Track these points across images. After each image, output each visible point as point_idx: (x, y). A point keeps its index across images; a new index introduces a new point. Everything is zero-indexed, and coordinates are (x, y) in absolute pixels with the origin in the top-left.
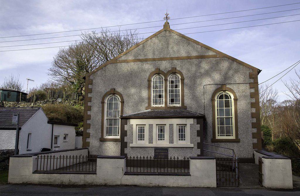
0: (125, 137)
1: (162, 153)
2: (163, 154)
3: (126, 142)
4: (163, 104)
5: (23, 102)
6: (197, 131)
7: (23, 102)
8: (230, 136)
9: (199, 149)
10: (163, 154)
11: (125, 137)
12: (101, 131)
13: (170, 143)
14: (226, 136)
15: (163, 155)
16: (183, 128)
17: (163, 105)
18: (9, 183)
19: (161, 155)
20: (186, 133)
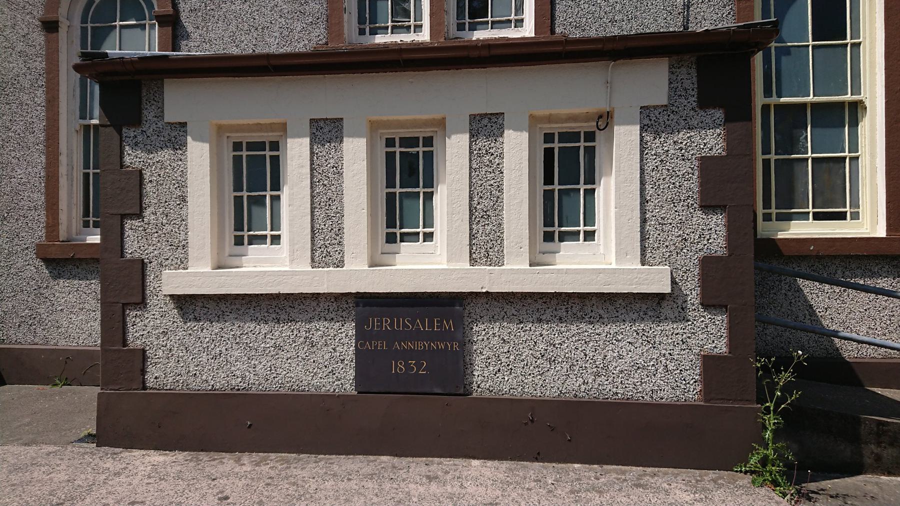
0: (128, 223)
1: (417, 336)
2: (420, 345)
3: (133, 261)
4: (418, 28)
5: (428, 130)
6: (703, 160)
7: (428, 130)
8: (842, 216)
9: (694, 374)
10: (420, 345)
11: (128, 223)
12: (47, 200)
13: (473, 261)
14: (817, 217)
15: (418, 355)
16: (245, 153)
17: (424, 36)
18: (672, 290)
19: (406, 355)
20: (541, 188)
